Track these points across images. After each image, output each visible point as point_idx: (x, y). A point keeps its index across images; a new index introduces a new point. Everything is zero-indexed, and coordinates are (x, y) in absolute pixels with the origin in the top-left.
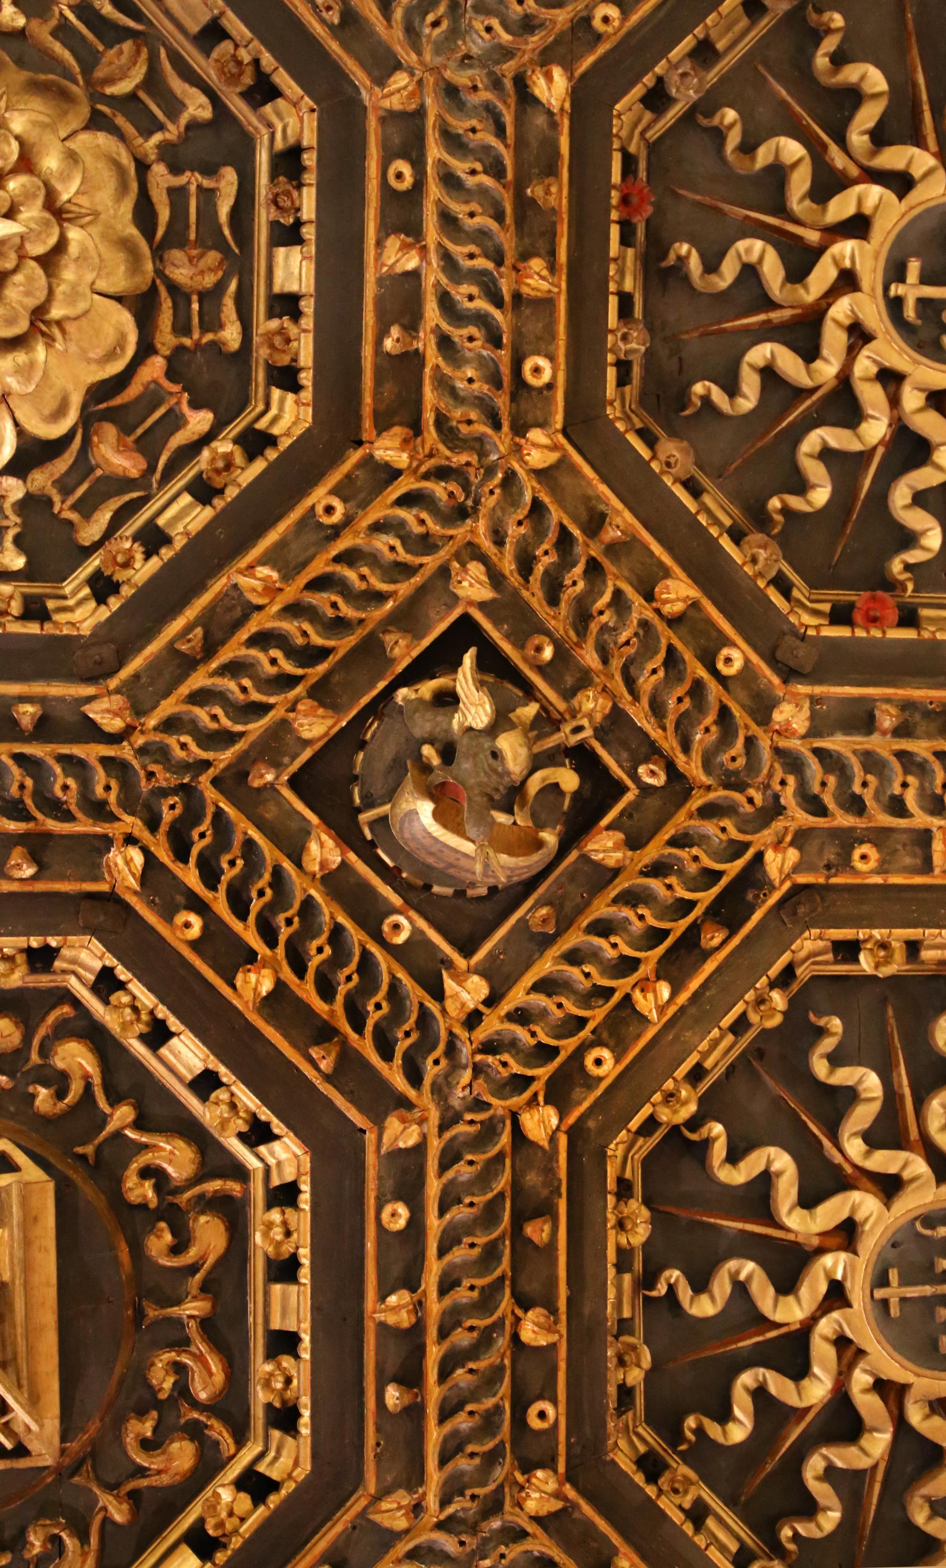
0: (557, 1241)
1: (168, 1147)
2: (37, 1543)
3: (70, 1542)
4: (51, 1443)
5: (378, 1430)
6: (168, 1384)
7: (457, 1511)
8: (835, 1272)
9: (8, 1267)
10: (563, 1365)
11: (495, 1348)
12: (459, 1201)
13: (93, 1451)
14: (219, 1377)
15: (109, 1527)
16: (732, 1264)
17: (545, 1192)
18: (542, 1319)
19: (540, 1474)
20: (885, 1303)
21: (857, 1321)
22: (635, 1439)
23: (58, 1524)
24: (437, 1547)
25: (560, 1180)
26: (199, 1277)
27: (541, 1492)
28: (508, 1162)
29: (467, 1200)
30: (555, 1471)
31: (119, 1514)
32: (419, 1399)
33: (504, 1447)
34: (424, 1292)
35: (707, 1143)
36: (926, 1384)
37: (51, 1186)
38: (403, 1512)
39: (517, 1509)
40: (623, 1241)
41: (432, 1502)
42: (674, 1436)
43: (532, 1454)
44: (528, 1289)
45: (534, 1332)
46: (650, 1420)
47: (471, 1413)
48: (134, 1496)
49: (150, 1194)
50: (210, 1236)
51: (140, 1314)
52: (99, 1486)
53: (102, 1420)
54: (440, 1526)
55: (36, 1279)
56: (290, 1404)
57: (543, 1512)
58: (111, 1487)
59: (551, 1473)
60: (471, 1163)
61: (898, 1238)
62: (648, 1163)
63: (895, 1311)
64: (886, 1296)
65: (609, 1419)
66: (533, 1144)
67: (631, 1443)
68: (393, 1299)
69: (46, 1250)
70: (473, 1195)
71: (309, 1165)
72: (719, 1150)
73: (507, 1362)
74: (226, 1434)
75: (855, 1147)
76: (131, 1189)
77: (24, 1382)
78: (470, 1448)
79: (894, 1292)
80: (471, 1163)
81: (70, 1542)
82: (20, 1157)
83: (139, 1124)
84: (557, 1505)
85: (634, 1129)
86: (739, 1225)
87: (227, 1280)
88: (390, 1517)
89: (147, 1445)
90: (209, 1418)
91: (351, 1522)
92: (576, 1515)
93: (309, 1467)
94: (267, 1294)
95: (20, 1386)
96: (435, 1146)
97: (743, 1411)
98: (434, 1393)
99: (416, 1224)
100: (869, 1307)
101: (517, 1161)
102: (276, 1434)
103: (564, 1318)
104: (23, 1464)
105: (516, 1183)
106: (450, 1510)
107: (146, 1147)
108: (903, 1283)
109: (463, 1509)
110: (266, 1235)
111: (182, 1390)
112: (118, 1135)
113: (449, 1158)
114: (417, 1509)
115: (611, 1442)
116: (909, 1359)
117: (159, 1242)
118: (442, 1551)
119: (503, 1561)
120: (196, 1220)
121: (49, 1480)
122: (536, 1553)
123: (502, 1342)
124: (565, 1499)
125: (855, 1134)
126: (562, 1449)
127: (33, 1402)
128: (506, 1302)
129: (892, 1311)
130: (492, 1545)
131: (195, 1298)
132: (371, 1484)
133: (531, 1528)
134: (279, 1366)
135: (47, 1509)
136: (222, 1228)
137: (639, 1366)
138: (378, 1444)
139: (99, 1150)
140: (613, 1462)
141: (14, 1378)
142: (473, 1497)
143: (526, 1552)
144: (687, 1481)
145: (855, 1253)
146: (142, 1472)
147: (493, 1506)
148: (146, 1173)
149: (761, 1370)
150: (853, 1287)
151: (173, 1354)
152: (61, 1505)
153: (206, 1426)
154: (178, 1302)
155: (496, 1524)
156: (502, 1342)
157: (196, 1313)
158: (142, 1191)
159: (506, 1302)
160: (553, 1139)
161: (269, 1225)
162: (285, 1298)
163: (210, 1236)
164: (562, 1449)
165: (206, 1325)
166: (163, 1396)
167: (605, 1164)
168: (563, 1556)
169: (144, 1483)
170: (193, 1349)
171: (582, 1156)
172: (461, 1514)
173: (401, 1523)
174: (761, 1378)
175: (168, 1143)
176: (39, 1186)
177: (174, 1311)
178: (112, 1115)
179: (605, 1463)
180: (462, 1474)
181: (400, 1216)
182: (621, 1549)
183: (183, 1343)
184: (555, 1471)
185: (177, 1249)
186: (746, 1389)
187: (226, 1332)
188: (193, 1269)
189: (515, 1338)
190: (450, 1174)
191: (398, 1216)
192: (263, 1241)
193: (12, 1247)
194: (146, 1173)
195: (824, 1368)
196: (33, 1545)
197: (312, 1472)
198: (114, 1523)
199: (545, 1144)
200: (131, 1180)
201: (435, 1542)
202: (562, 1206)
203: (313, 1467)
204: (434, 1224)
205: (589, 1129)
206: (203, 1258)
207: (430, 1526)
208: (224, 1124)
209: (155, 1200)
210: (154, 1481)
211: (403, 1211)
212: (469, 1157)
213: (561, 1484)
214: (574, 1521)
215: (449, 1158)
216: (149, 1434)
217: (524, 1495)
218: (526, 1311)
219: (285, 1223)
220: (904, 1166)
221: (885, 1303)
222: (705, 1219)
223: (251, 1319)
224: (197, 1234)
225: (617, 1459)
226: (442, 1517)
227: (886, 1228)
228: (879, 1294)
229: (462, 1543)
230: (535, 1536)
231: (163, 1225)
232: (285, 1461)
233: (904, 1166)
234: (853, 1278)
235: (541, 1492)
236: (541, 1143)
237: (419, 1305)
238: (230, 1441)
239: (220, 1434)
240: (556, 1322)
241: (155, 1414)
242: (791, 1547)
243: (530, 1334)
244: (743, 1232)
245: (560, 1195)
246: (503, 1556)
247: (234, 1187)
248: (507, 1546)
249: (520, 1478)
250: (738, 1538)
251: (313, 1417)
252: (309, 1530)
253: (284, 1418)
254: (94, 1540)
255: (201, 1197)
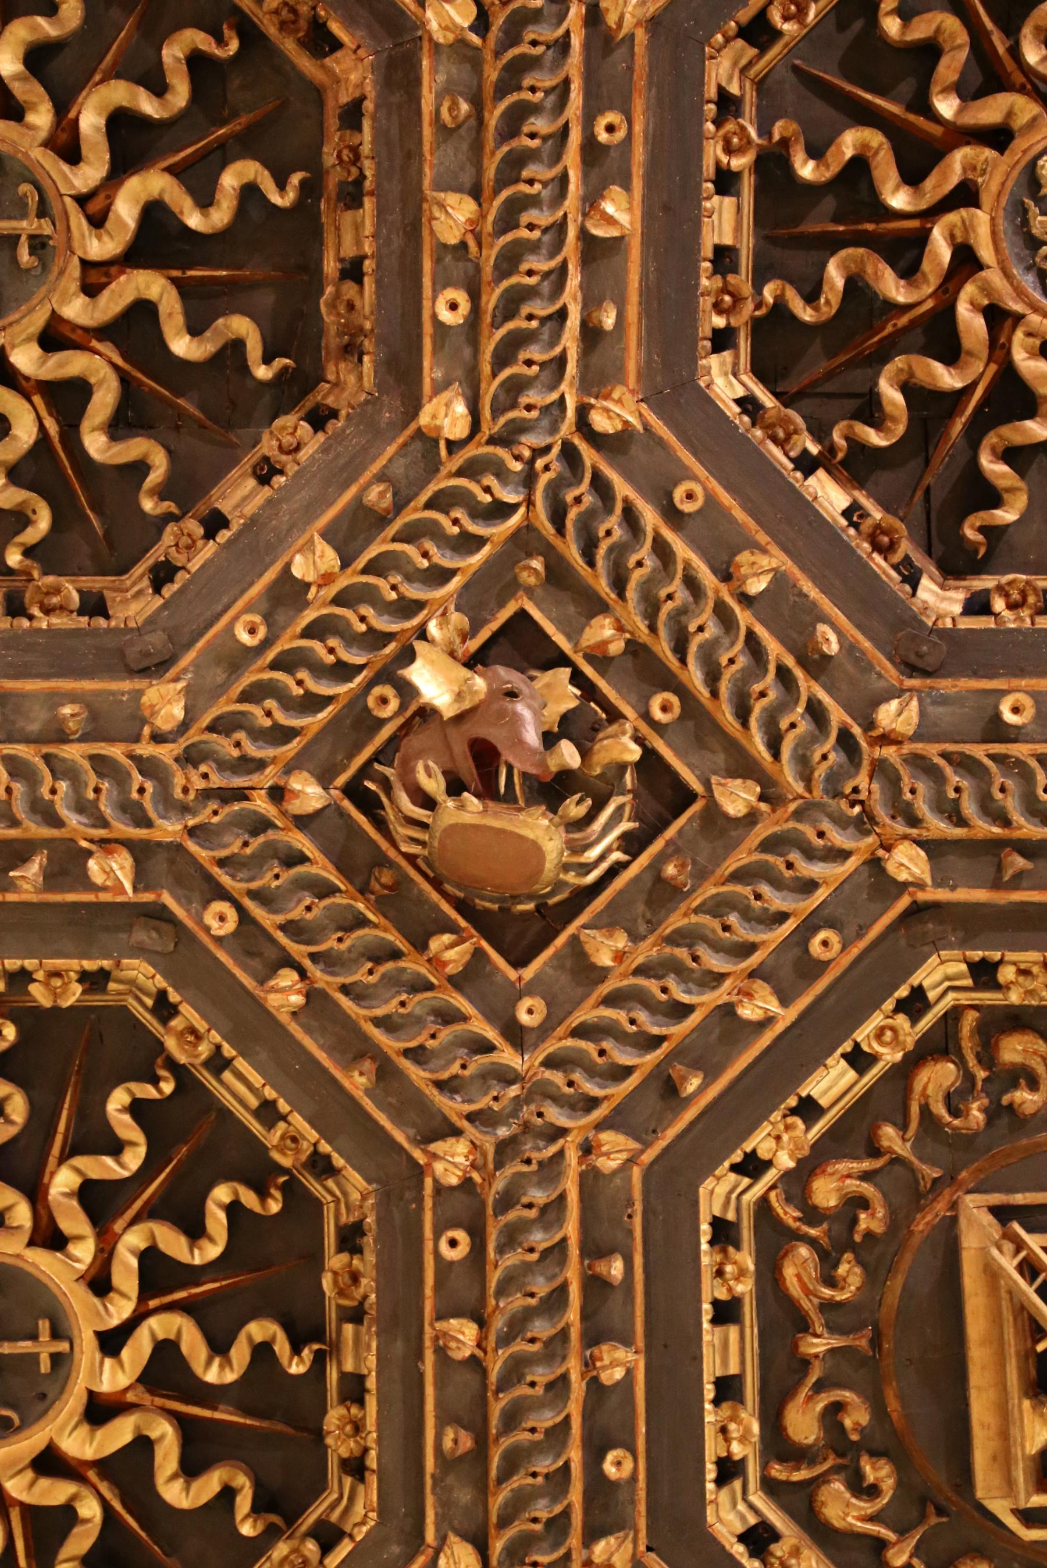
0: (436, 1427)
1: (850, 1519)
2: (975, 1113)
3: (940, 1109)
4: (969, 1220)
5: (630, 1233)
6: (842, 1269)
7: (546, 1148)
8: (112, 1367)
9: (1025, 1415)
10: (428, 1291)
11: (507, 1316)
12: (547, 1476)
13: (918, 1201)
14: (789, 1272)
15: (899, 1120)
16: (230, 1377)
17: (450, 1480)
18: (453, 1344)
19: (454, 1181)
20: (56, 1335)
21: (89, 1316)
22: (338, 1193)
23: (954, 1129)
24: (567, 1111)
25: (433, 1493)
26: (813, 1379)
27: (452, 1161)
28: (494, 1519)
29: (540, 1480)
30: (436, 1181)
31: (889, 1135)
32: (586, 1262)
33: (494, 1210)
34: (583, 1379)
35: (257, 1509)
36: (11, 1247)
37: (980, 1494)
38: (604, 1149)
39: (478, 1143)
40: (354, 1410)
41: (572, 1156)
42: (292, 1190)
43: (466, 1206)
44: (469, 1376)
45: (463, 1333)
46: (317, 1205)
47: (531, 1250)
48: (875, 1151)
49: (868, 1469)
50: (803, 1423)
51: (876, 1342)
52: (912, 1163)
53: (911, 1233)
54: (563, 1132)
55: (991, 1395)
56: (717, 1248)
57: (451, 1140)
58: (897, 1160)
59: (443, 1181)
60: (535, 1520)
61: (41, 1406)
62: (319, 1486)
63: (44, 1326)
64: (54, 1343)
65: (374, 1227)
66: (465, 1537)
67: (345, 1194)
68: (618, 1374)
69: (982, 1425)
70: (533, 1486)
71: (708, 1512)
72: (244, 1503)
73: (492, 1302)
74: (780, 1211)
75: (90, 1509)
76: (888, 1476)
77: (1004, 1295)
78: (533, 1213)
79: (44, 1349)
80: (535, 1520)
81: (940, 1109)
82: (1012, 1522)
83: (880, 1545)
84: (433, 1147)
85: (346, 1540)
86: (217, 1415)
87: (782, 1376)
88: (618, 1144)
89: (861, 1203)
90: (798, 1229)
91: (658, 1139)
92: (412, 1132)
93: (701, 1190)
94: (743, 1362)
95: (1010, 1292)
96: (574, 1540)
97: (216, 1219)
98: (572, 1274)
99: (595, 1454)
100: (76, 1332)
101: (481, 1515)
102: (731, 1216)
103: (428, 1343)
104: (997, 1198)
105: (483, 1491)
106: (553, 1149)
107: (871, 1519)
108: (35, 1358)
109: (539, 1150)
110: (748, 1430)
111: (828, 1260)
112: (903, 1531)
113: (558, 1525)
114: (587, 1149)
115: (371, 1201)
116: (29, 1274)
117: (857, 1417)
118: (562, 1107)
119: (495, 1094)
120: (816, 1440)
121: (964, 1174)
122: (458, 1098)
123: (498, 1324)
124: (425, 1152)
125: (87, 1521)
126: (428, 1203)
127: (992, 1273)
128: (495, 1370)
129: (47, 1324)
130: (508, 1110)
131: (816, 1356)
132: (636, 1172)
133: (465, 1124)
134: (730, 1290)
135: (965, 1145)
136: (790, 1431)
137: (335, 1273)
138: (630, 1216)
139: (923, 1517)
140: (369, 1181)
141: (1015, 1300)
142: (528, 1162)
143: (470, 1101)
144: (281, 1149)
145: (91, 1394)
146: (865, 1176)
147: (505, 1150)
148: (872, 1491)
149: (197, 1261)
150: (93, 1353)
151: (838, 1298)
152: (950, 1145)
153: (799, 1219)
154: (832, 1351)
155: (503, 1132)
156: (498, 1324)
157: (815, 1341)
158: (877, 1472)
159: (495, 1370)
160: (443, 1540)
161: (743, 1439)
162: (725, 1362)
163: (803, 1423)
164: (428, 1203)
165: (803, 1326)
166: (848, 1256)
167: (379, 1504)
168: (427, 1092)
169: (866, 1165)
170: (816, 1301)
171: (406, 1515)
172: (541, 1144)
173: (608, 1138)
174: (196, 1252)
175: (850, 1524)
176: (991, 1494)
177: (836, 1342)
178: (910, 1557)
179: (378, 1182)
180: (539, 1184)
181: (612, 1463)
182: (361, 1094)
183: (827, 1307)
184: (436, 1181)
185: (837, 1408)
186: (212, 1240)
187: (783, 1321)
188: (819, 1387)
189: (482, 1323)
190: (558, 1509)
191: (615, 1466)
192: (750, 1424)
193: (1023, 1438)
194: (872, 1491)
195: (126, 1266)
196: (979, 1110)
197: (698, 1187)
198: (894, 1124)
199: (453, 1538)
200: (888, 1485)
201: (570, 1117)
202: (430, 1463)
203: (697, 1192)
204: (575, 1455)
205: (399, 1544)
206: (809, 1399)
207: (574, 1133)
208: (796, 1552)
209: (862, 1463)
210: (856, 1166)
211: (609, 1469)
212: (538, 1527)
213: (429, 1165)
214: (414, 1125)
215: (558, 1525)
216: (863, 1216)
217: (471, 1157)
218: (473, 1356)
219: (728, 1440)
220: (32, 1484)
221: (56, 1335)
222: (256, 1423)
223: (756, 1330)
224: (816, 1424)
225: (364, 1183)
226: (561, 1142)
227: (54, 1419)
228: (63, 1347)
229: (540, 1115)
230: (460, 1115)
231: (855, 1437)
232: (722, 1189)
233: (32, 1484)
234: (93, 1364)
235: (452, 1161)
236: (457, 1539)
237: (589, 1364)
238: (775, 1204)
239: (786, 1213)
240: (436, 1338)
241: (858, 1238)
242: (163, 1073)
243: (467, 1332)
244: (215, 1409)
245: (433, 1476)
246: (496, 1099)
247: (778, 1472)
248: (490, 1108)
249: (476, 1177)
250: (221, 1082)
251: (698, 1244)
252: (700, 1126)
253: (724, 1233)
254: (915, 1109)
255: (812, 1463)
